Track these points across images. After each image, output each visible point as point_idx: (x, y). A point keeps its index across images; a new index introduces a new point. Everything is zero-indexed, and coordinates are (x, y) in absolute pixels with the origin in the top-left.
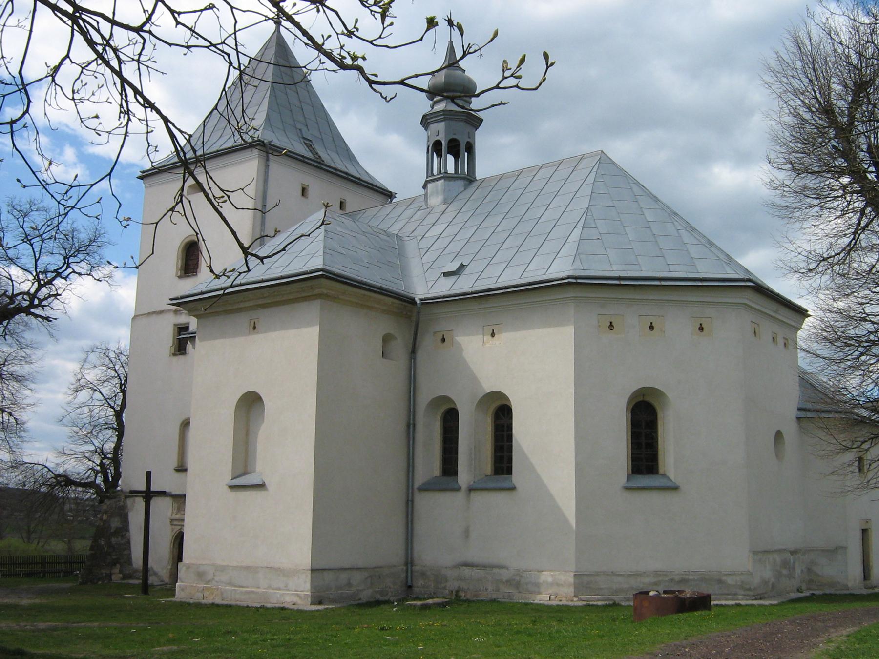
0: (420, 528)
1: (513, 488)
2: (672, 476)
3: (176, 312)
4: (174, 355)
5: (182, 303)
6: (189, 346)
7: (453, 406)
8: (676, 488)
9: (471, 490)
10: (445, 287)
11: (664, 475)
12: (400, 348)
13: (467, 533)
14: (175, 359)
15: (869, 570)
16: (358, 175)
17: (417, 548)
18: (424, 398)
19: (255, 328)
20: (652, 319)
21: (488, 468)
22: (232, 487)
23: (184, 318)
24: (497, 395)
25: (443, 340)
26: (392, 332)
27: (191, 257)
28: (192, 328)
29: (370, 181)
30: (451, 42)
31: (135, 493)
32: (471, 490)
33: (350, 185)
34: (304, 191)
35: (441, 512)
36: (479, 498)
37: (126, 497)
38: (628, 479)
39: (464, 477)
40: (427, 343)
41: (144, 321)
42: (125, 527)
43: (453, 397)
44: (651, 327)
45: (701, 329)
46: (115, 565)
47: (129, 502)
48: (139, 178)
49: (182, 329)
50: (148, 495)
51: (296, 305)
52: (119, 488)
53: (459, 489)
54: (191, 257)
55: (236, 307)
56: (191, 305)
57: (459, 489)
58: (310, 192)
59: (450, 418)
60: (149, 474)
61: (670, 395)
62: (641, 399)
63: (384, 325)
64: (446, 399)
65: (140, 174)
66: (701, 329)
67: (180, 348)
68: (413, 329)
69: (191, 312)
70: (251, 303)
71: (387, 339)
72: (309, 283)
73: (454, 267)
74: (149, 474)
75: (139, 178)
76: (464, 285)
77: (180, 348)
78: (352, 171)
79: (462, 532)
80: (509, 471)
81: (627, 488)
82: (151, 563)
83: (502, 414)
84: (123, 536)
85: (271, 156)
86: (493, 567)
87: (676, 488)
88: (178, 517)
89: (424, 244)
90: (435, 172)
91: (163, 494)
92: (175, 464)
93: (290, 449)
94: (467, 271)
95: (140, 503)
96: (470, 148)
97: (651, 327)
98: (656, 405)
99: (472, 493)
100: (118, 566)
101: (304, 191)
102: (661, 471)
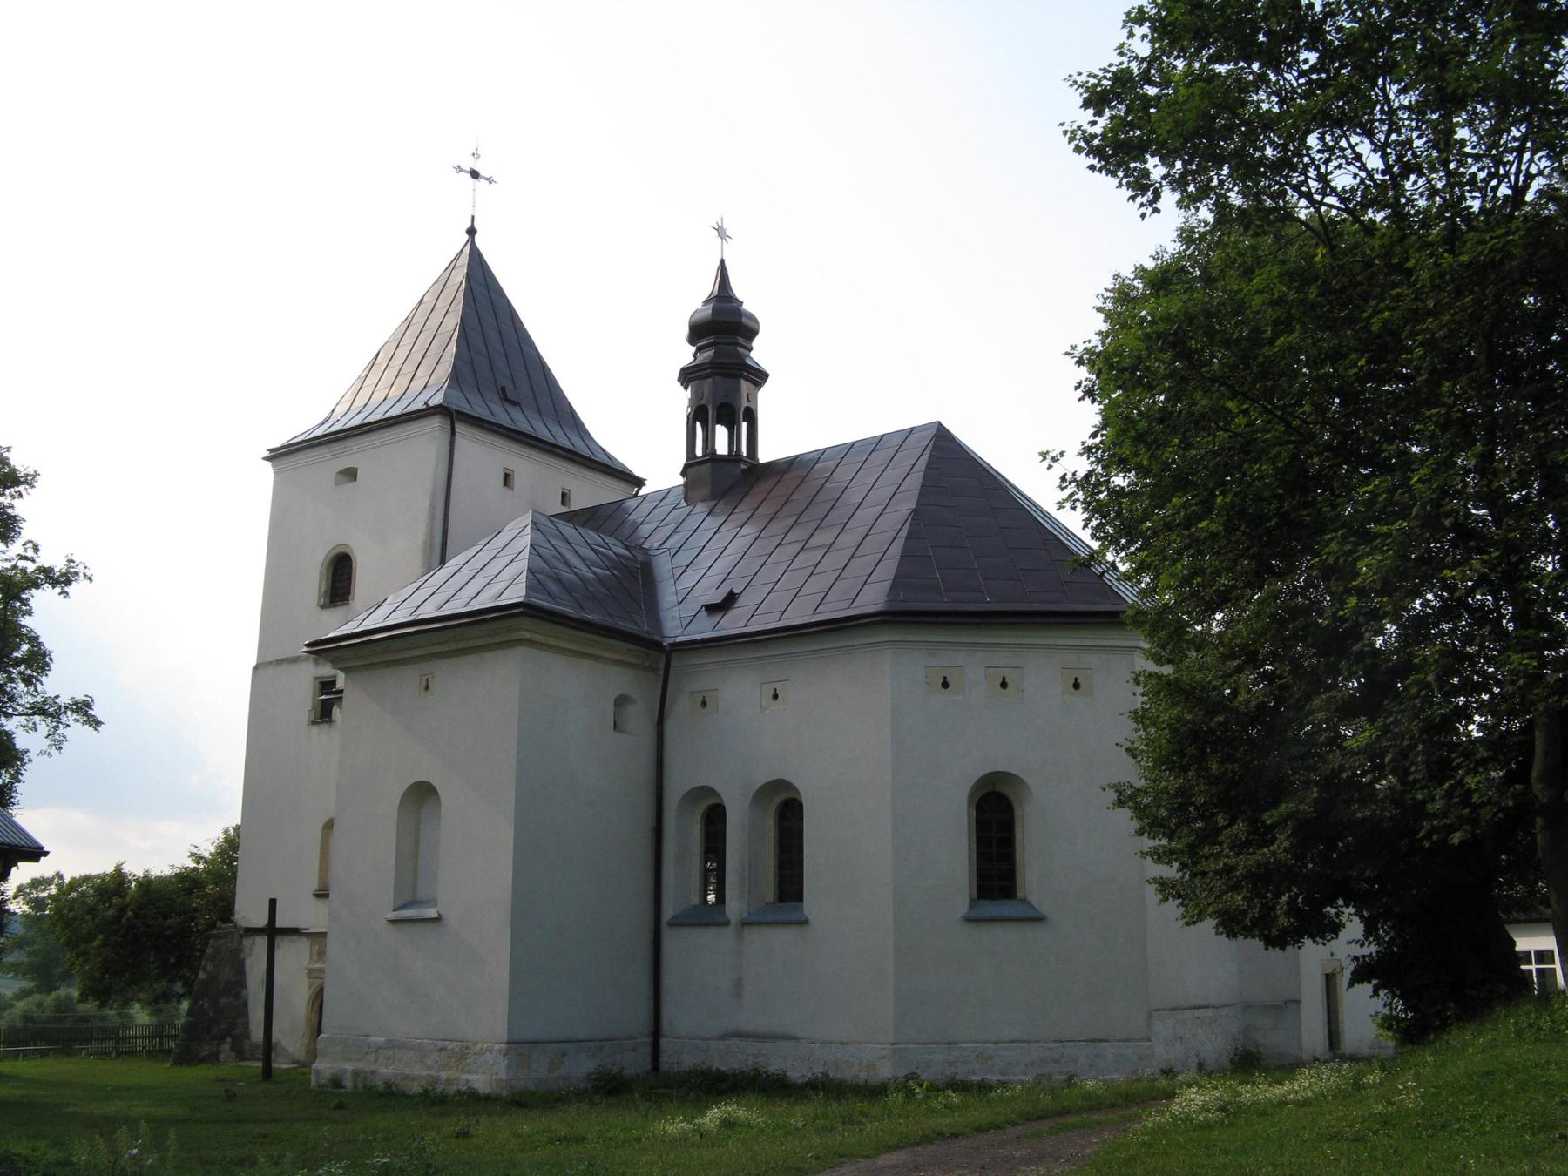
0: (670, 981)
1: (805, 922)
2: (1034, 899)
3: (316, 662)
4: (314, 723)
5: (321, 649)
6: (336, 711)
7: (711, 801)
8: (1039, 919)
9: (745, 924)
10: (705, 628)
11: (1025, 901)
12: (639, 717)
13: (738, 988)
14: (315, 729)
15: (1338, 1034)
16: (589, 454)
17: (667, 1011)
18: (676, 789)
19: (427, 687)
20: (1005, 672)
21: (769, 890)
22: (392, 921)
23: (327, 670)
24: (779, 785)
25: (704, 704)
26: (628, 693)
27: (339, 578)
28: (340, 685)
29: (607, 461)
30: (722, 261)
31: (252, 932)
32: (745, 924)
33: (575, 469)
34: (507, 479)
35: (696, 958)
36: (757, 938)
37: (241, 937)
38: (971, 907)
39: (735, 907)
40: (681, 707)
41: (270, 670)
42: (239, 983)
43: (711, 784)
44: (1004, 685)
45: (1076, 686)
46: (224, 1038)
47: (247, 942)
48: (266, 459)
49: (327, 686)
50: (272, 932)
51: (488, 655)
52: (1351, 939)
53: (727, 923)
54: (339, 578)
55: (400, 656)
56: (337, 654)
57: (727, 923)
58: (518, 480)
59: (715, 818)
60: (273, 902)
61: (1032, 782)
62: (989, 789)
63: (619, 680)
64: (705, 791)
65: (267, 454)
66: (1076, 686)
67: (324, 713)
68: (660, 684)
69: (335, 663)
70: (421, 652)
71: (621, 702)
72: (507, 623)
73: (718, 597)
74: (273, 902)
75: (266, 459)
76: (732, 623)
77: (324, 713)
78: (581, 448)
79: (733, 988)
80: (798, 896)
81: (969, 920)
82: (276, 1035)
83: (787, 812)
84: (237, 996)
85: (459, 427)
86: (775, 1037)
87: (1039, 919)
88: (318, 965)
89: (683, 559)
90: (699, 452)
91: (294, 931)
92: (314, 885)
93: (478, 867)
94: (741, 601)
95: (261, 943)
96: (751, 416)
97: (1004, 685)
98: (1012, 797)
99: (746, 929)
100: (229, 1040)
101: (507, 479)
102: (1020, 894)
